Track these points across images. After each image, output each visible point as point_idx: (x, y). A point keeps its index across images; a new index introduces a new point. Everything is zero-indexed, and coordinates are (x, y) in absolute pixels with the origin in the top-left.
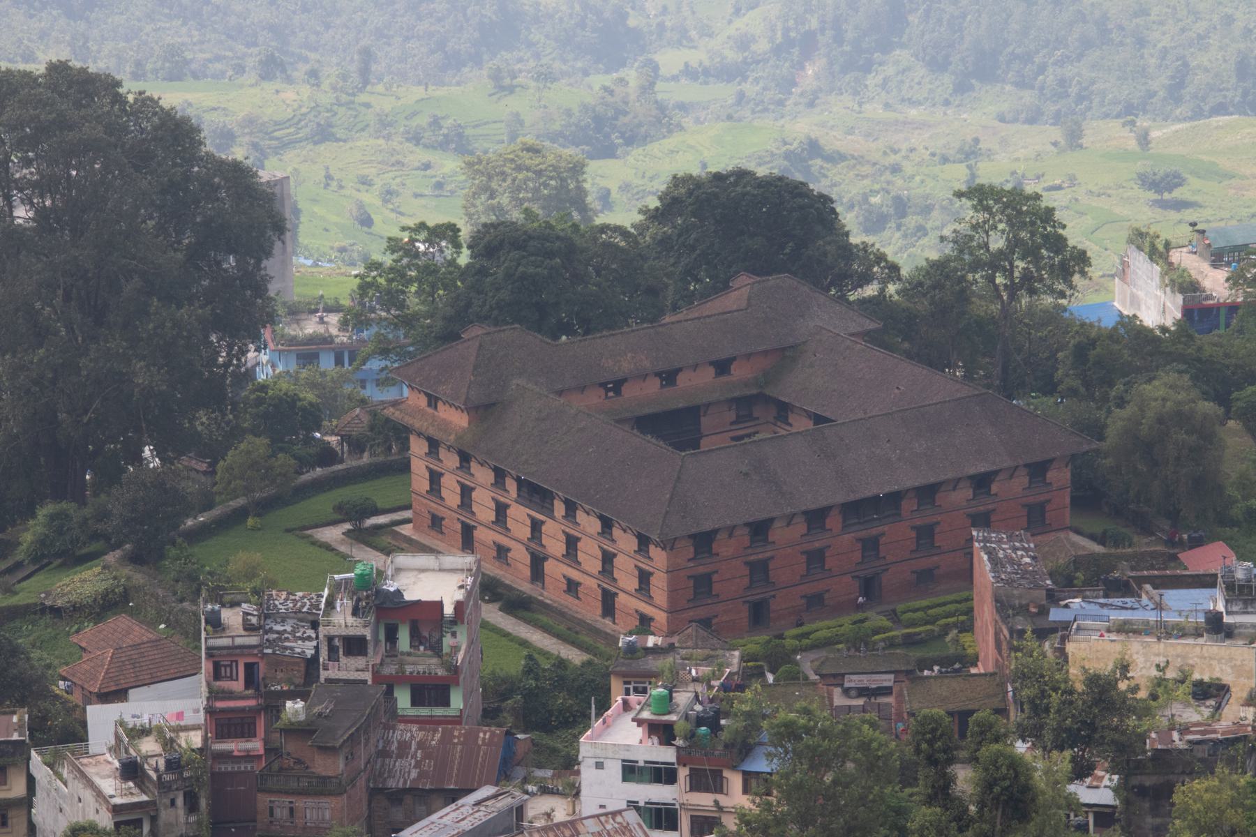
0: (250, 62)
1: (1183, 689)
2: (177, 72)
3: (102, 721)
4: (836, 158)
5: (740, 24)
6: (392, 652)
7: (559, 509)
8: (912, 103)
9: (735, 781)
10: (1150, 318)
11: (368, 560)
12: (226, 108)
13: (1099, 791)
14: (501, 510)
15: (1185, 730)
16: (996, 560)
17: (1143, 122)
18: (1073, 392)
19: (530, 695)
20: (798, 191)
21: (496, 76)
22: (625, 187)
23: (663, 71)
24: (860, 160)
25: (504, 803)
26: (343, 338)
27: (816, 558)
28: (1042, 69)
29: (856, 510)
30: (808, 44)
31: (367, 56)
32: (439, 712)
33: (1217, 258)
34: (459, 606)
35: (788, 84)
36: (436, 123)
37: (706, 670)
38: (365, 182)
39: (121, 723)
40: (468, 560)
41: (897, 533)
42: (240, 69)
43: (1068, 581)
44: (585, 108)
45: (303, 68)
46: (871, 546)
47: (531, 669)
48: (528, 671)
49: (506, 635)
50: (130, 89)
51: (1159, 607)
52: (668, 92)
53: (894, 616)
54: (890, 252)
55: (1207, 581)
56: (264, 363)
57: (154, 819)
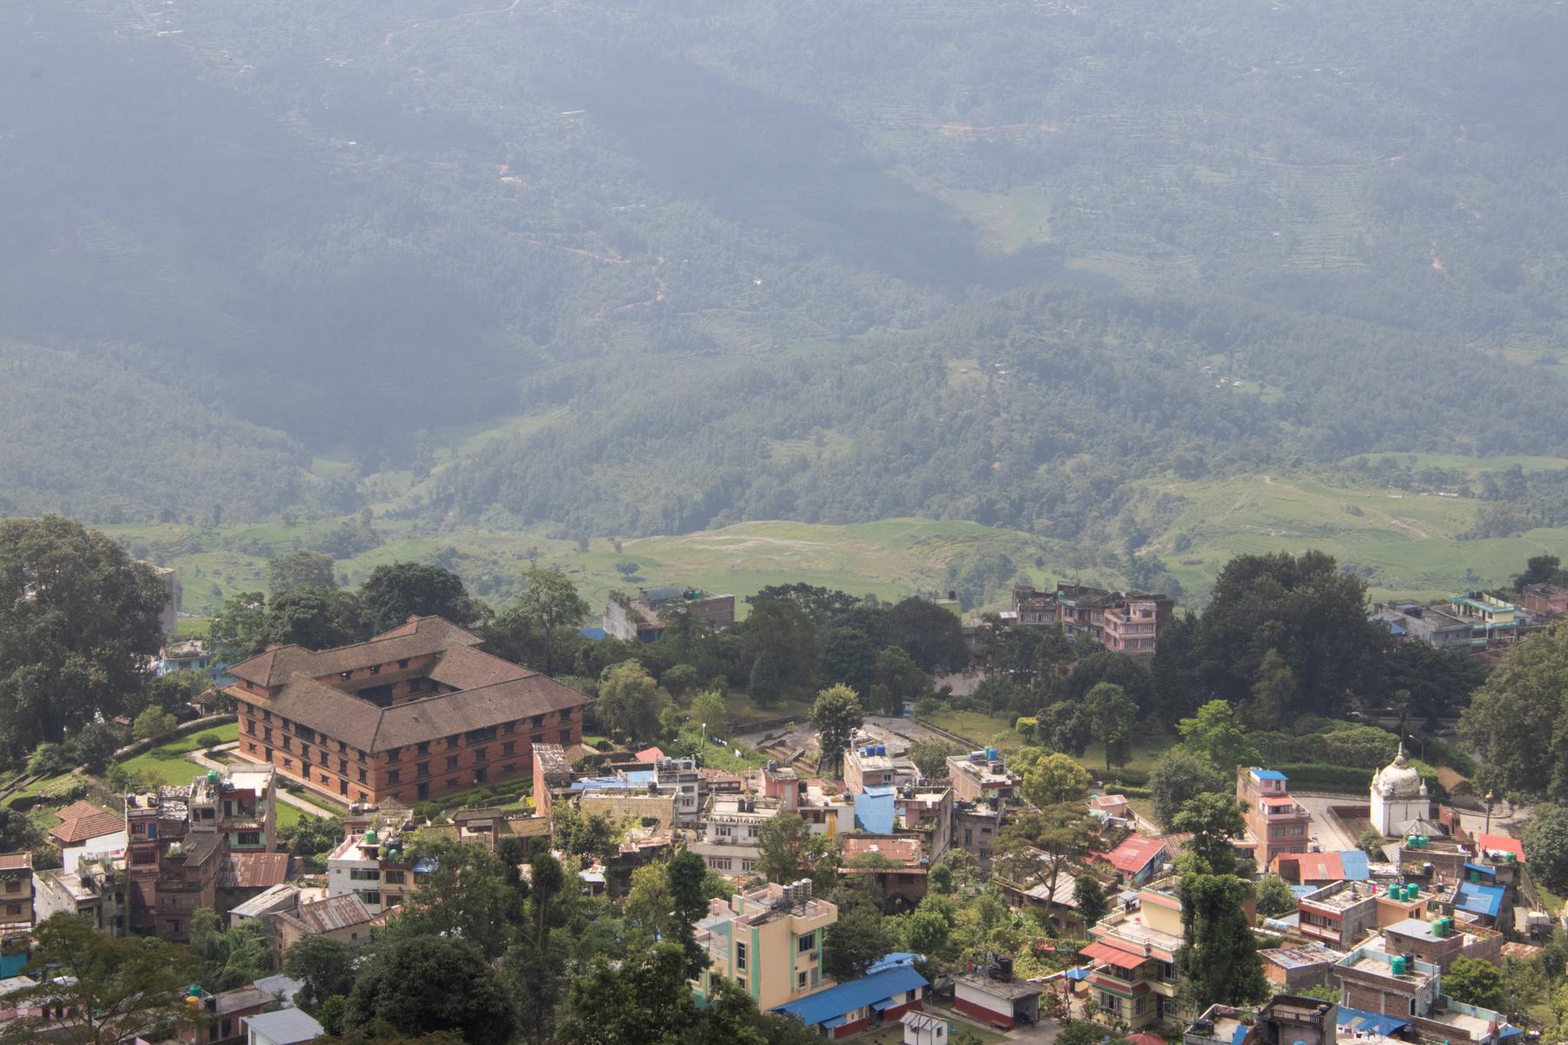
0: (156, 514)
1: (639, 821)
2: (117, 518)
3: (71, 857)
4: (465, 557)
5: (414, 490)
6: (228, 813)
7: (318, 739)
8: (504, 529)
9: (410, 877)
10: (621, 636)
11: (215, 767)
12: (141, 537)
13: (596, 874)
14: (287, 740)
15: (638, 842)
16: (546, 758)
17: (618, 539)
18: (583, 674)
19: (303, 836)
20: (441, 573)
21: (287, 518)
22: (356, 573)
23: (375, 514)
24: (477, 558)
25: (288, 893)
26: (204, 653)
27: (453, 761)
28: (568, 512)
29: (475, 736)
30: (449, 500)
31: (218, 508)
32: (253, 846)
33: (653, 605)
34: (264, 791)
35: (440, 520)
36: (255, 542)
37: (395, 820)
38: (217, 573)
39: (81, 857)
40: (269, 766)
41: (494, 748)
42: (151, 517)
43: (582, 768)
44: (334, 533)
45: (184, 516)
46: (481, 754)
47: (303, 821)
48: (301, 824)
49: (289, 805)
50: (89, 530)
51: (626, 781)
52: (378, 525)
53: (493, 790)
54: (491, 605)
55: (649, 767)
56: (159, 665)
57: (99, 907)
